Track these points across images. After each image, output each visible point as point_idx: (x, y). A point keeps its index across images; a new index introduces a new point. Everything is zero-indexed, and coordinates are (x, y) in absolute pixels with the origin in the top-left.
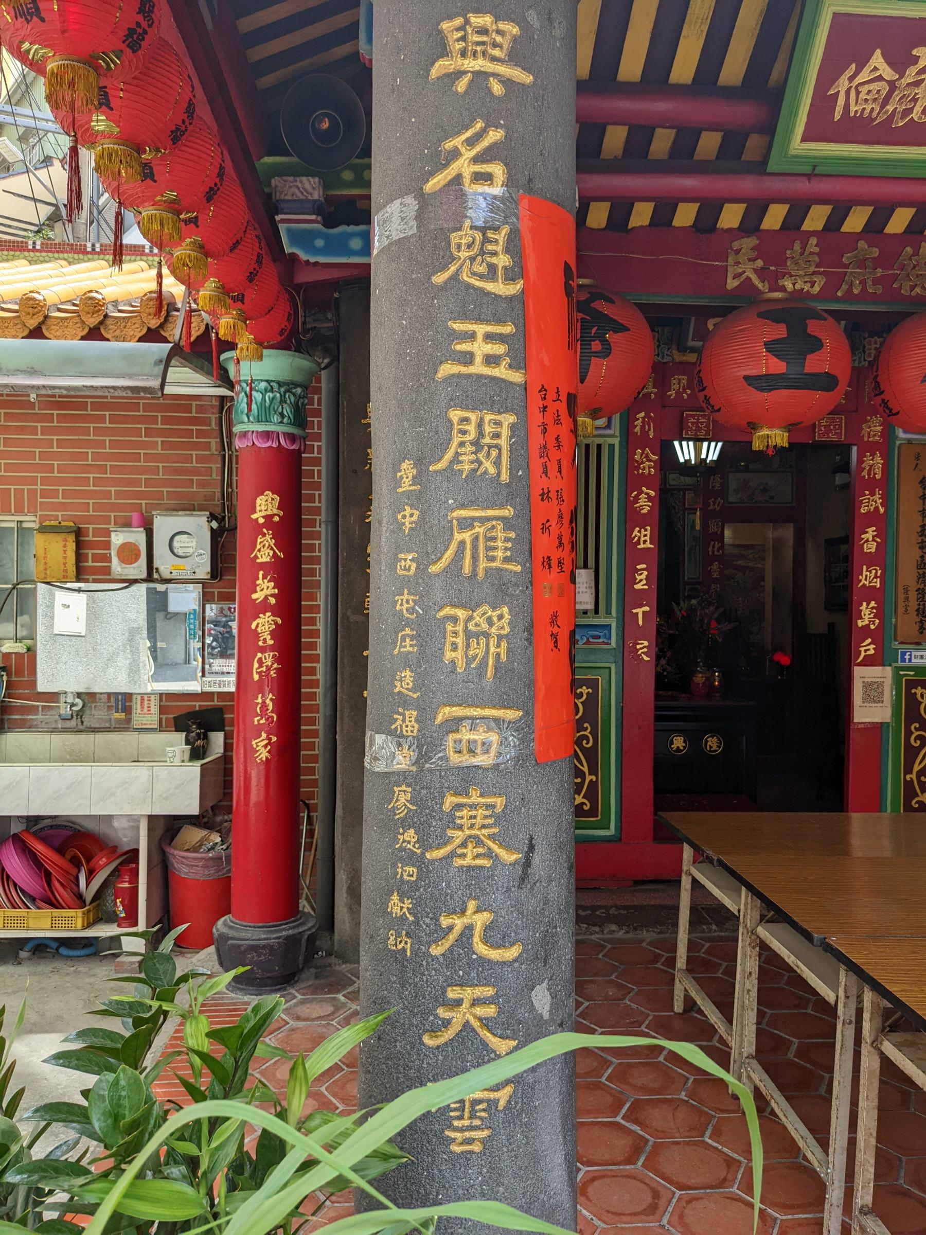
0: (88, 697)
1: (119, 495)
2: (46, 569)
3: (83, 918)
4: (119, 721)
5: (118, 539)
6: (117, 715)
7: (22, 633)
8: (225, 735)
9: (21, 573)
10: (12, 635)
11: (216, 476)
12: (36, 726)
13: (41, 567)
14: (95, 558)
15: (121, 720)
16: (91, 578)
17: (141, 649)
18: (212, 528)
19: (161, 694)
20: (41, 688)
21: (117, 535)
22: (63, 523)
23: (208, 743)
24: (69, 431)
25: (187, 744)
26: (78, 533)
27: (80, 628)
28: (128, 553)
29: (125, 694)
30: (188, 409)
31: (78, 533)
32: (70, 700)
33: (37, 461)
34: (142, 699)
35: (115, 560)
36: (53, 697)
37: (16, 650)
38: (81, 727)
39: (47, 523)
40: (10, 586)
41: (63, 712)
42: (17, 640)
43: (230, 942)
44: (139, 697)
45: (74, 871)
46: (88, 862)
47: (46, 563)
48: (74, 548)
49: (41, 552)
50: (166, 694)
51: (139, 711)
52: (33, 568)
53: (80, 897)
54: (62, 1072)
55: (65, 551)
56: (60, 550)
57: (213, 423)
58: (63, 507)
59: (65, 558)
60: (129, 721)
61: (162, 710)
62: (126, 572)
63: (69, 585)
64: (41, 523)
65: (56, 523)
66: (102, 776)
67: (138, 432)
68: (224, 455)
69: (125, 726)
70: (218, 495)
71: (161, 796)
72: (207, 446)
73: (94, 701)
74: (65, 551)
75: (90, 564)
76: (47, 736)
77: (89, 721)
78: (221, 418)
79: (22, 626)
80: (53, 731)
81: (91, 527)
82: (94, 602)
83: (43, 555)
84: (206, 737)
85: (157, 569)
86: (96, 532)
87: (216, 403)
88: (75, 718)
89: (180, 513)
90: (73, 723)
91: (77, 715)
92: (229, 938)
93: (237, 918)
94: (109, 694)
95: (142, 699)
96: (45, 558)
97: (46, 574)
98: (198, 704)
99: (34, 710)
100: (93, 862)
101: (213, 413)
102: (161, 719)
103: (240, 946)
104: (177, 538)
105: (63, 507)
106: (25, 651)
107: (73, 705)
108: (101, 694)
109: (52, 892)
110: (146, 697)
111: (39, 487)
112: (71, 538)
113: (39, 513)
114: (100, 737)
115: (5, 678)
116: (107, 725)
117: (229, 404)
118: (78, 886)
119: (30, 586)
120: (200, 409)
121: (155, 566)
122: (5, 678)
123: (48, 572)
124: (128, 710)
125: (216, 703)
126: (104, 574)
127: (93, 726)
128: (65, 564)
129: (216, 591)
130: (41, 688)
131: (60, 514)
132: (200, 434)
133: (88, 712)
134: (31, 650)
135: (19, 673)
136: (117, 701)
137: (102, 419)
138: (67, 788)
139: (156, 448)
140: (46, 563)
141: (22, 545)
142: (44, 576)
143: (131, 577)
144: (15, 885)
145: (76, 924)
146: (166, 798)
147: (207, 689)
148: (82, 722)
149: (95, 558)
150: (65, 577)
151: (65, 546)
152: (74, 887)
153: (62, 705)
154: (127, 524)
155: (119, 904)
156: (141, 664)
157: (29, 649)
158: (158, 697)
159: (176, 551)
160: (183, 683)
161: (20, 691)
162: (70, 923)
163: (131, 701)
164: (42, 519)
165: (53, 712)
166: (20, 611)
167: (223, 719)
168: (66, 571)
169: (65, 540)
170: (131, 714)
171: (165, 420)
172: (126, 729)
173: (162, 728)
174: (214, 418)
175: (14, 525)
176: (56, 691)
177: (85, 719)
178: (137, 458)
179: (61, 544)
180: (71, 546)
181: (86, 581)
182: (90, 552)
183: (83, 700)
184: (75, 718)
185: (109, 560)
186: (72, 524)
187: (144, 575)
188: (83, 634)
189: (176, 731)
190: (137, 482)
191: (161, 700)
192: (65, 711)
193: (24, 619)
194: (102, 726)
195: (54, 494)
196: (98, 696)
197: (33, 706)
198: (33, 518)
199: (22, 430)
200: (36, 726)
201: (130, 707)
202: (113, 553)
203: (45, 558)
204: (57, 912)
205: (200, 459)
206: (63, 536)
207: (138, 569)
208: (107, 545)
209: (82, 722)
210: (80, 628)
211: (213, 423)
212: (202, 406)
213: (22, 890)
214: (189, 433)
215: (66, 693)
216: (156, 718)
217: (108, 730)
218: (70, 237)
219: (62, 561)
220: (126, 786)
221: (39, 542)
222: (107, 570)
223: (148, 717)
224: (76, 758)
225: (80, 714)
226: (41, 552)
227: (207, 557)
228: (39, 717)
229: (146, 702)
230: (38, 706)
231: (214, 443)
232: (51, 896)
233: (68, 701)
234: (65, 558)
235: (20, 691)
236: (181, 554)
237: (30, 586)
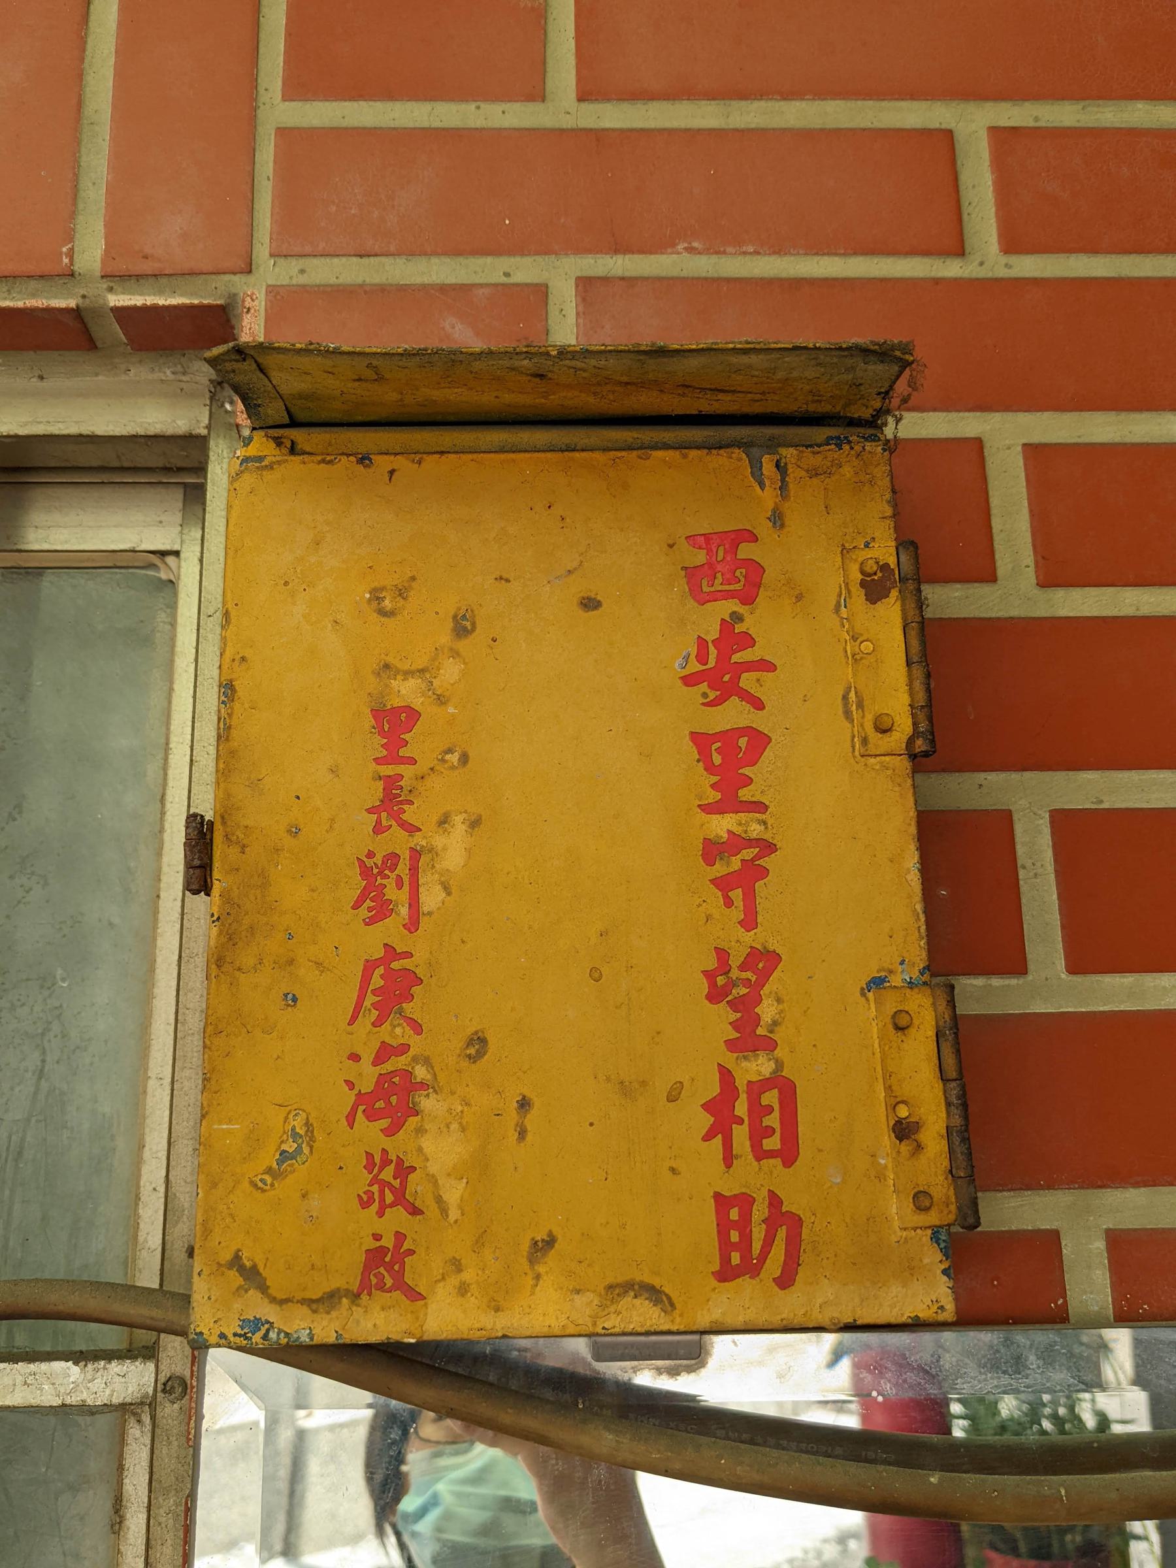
2: (392, 1099)
13: (314, 1056)
47: (392, 986)
49: (321, 781)
54: (772, 1350)
55: (730, 760)
59: (740, 870)
74: (730, 760)
83: (356, 834)
89: (915, 644)
96: (380, 884)
97: (391, 1185)
128: (738, 984)
140: (392, 986)
142: (348, 1228)
151: (724, 668)
160: (377, 279)
169: (726, 568)
179: (665, 630)
203: (380, 884)
206: (696, 489)
219: (686, 924)
234: (740, 870)
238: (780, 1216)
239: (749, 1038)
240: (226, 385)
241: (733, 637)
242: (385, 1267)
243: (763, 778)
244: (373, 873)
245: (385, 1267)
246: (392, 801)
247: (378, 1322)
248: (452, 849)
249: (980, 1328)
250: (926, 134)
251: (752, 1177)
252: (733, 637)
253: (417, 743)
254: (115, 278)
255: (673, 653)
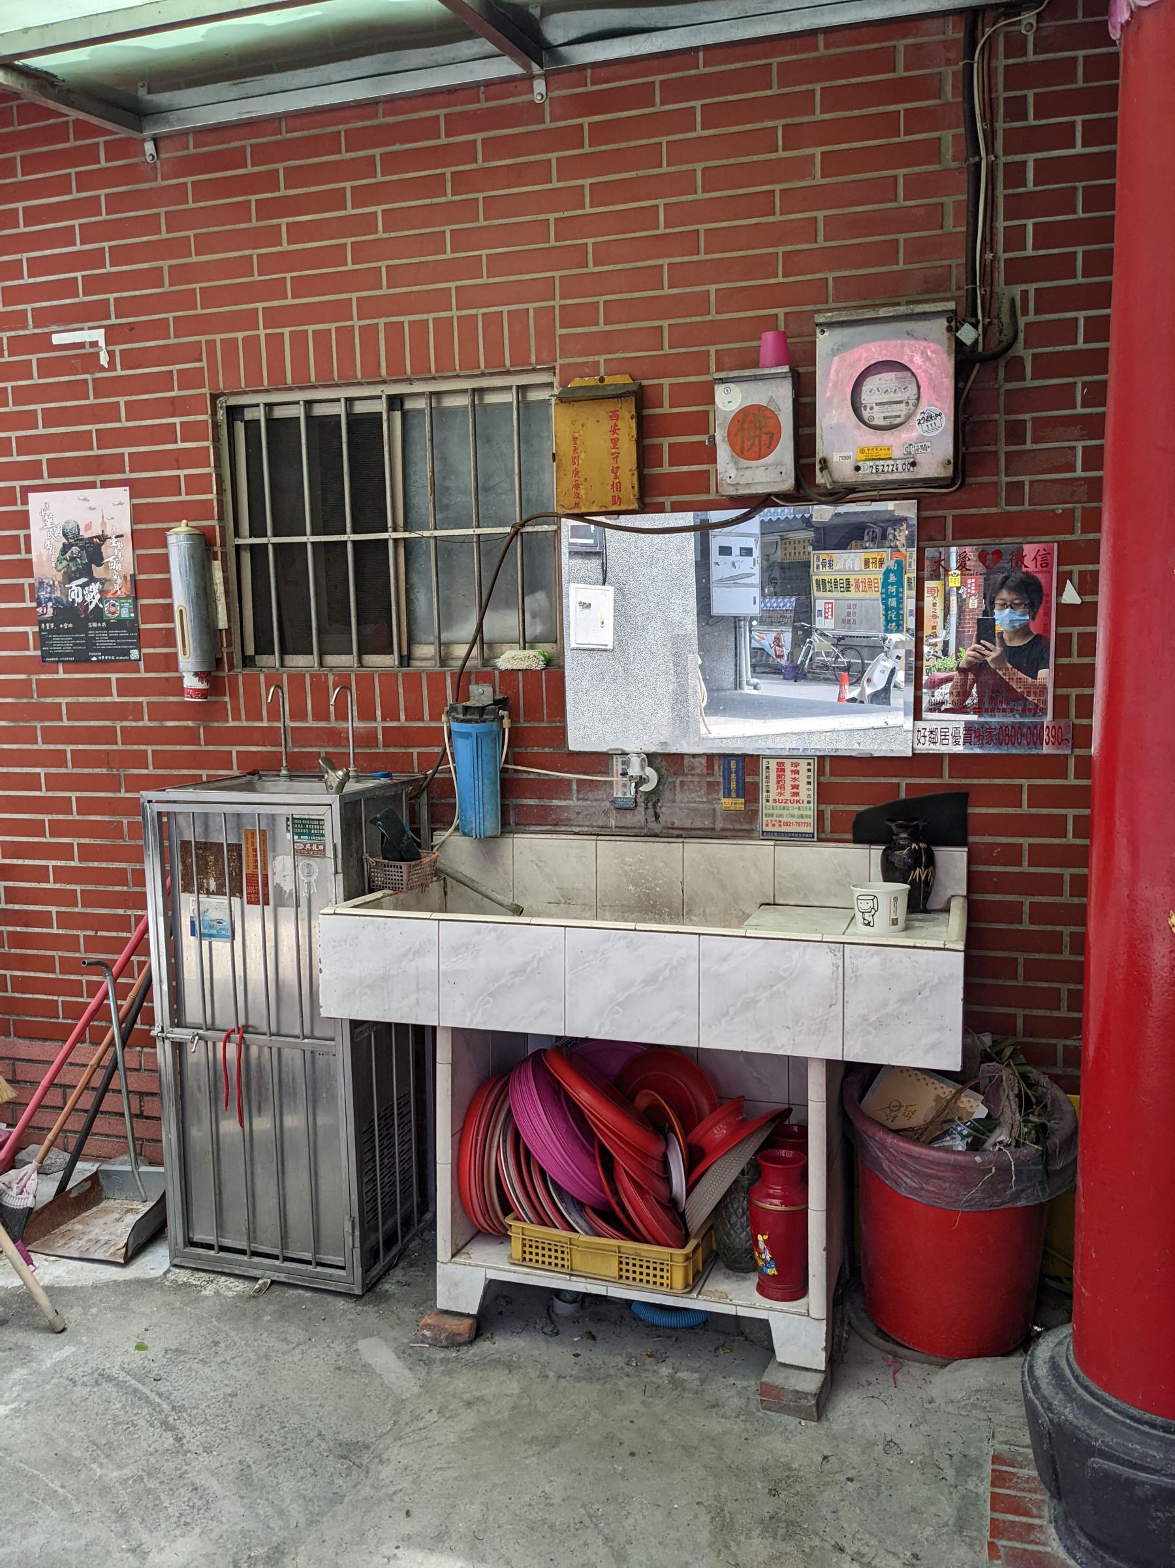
0: (667, 763)
1: (727, 300)
2: (577, 486)
3: (686, 1268)
4: (730, 815)
5: (729, 400)
6: (727, 803)
7: (535, 629)
8: (969, 853)
9: (529, 501)
10: (516, 633)
11: (953, 226)
12: (568, 822)
13: (568, 481)
14: (680, 455)
15: (736, 813)
16: (667, 500)
17: (690, 668)
18: (959, 343)
19: (821, 759)
20: (574, 745)
21: (728, 391)
22: (609, 380)
23: (934, 873)
24: (618, 160)
25: (887, 878)
26: (641, 398)
27: (606, 638)
28: (753, 432)
29: (744, 756)
30: (885, 61)
31: (641, 398)
32: (635, 770)
33: (553, 243)
34: (781, 770)
35: (723, 452)
36: (598, 761)
37: (524, 665)
38: (653, 825)
39: (577, 382)
40: (508, 530)
41: (618, 793)
42: (526, 643)
43: (1097, 1462)
44: (773, 764)
45: (656, 1150)
46: (687, 1129)
47: (576, 473)
48: (634, 433)
49: (566, 448)
50: (834, 758)
51: (773, 795)
52: (553, 488)
53: (673, 1208)
55: (615, 442)
56: (599, 444)
57: (948, 88)
58: (606, 342)
59: (616, 456)
60: (752, 815)
61: (824, 793)
62: (748, 476)
63: (624, 520)
64: (563, 385)
65: (593, 381)
66: (724, 960)
67: (766, 140)
68: (978, 166)
69: (744, 826)
70: (958, 274)
71: (865, 1018)
72: (932, 151)
73: (680, 772)
74: (615, 442)
75: (666, 469)
76: (589, 844)
77: (671, 813)
78: (970, 67)
79: (534, 616)
80: (601, 832)
81: (666, 382)
82: (624, 597)
84: (931, 862)
85: (824, 462)
86: (680, 394)
87: (954, 32)
88: (641, 809)
90: (638, 818)
91: (647, 801)
92: (1092, 1451)
93: (1079, 1363)
94: (710, 757)
95: (781, 770)
96: (575, 460)
97: (577, 496)
98: (903, 782)
99: (561, 789)
100: (697, 1133)
101: (948, 62)
102: (820, 815)
103: (1131, 1483)
104: (871, 383)
105: (606, 342)
106: (541, 665)
107: (641, 781)
108: (694, 756)
109: (616, 1193)
110: (788, 762)
111: (557, 302)
112: (627, 411)
113: (560, 361)
114: (694, 850)
115: (506, 723)
116: (707, 823)
117: (989, 31)
118: (668, 1180)
119: (546, 528)
120: (917, 56)
121: (820, 453)
122: (506, 723)
123: (582, 492)
124: (750, 793)
125: (946, 780)
126: (694, 491)
127: (677, 824)
128: (615, 471)
129: (949, 514)
130: (574, 745)
131: (601, 359)
132: (916, 120)
133: (668, 795)
134: (554, 668)
135: (533, 712)
136: (727, 771)
137: (684, 120)
138: (646, 983)
139: (807, 174)
140: (576, 473)
141: (527, 441)
143: (760, 490)
144: (543, 1174)
145: (670, 1278)
146: (880, 1024)
147: (926, 747)
148: (657, 816)
149: (680, 455)
150: (616, 500)
151: (614, 430)
152: (661, 1186)
153: (617, 779)
154: (745, 364)
155: (762, 1245)
156: (690, 691)
157: (548, 662)
158: (814, 766)
159: (866, 414)
161: (536, 750)
162: (653, 1277)
163: (756, 772)
164: (568, 372)
165: (600, 794)
166: (531, 584)
167: (965, 817)
168: (617, 486)
169: (615, 416)
170: (756, 800)
171: (832, 100)
172: (747, 834)
173: (824, 833)
174: (950, 74)
175: (509, 398)
176: (604, 750)
177: (665, 810)
178: (765, 203)
179: (607, 425)
180: (628, 428)
181: (660, 509)
182: (666, 442)
183: (657, 770)
184: (641, 809)
185: (710, 455)
186: (626, 379)
187: (787, 483)
188: (610, 647)
189: (855, 842)
190: (764, 266)
191: (821, 771)
192: (623, 791)
193: (537, 600)
194: (698, 824)
195: (587, 315)
196: (686, 760)
197: (561, 780)
198: (544, 378)
199: (518, 174)
200: (568, 822)
201: (756, 785)
202: (720, 436)
204: (629, 1245)
205: (916, 187)
206: (610, 406)
207: (774, 470)
208: (702, 422)
209: (657, 816)
210: (606, 638)
211: (948, 88)
212: (919, 47)
213: (554, 1183)
214: (888, 125)
215: (624, 754)
216: (810, 811)
217: (710, 834)
218: (544, 378)
219: (609, 463)
220: (780, 987)
221: (560, 424)
222: (702, 482)
223: (794, 809)
224: (655, 905)
225: (653, 798)
226: (566, 448)
227: (945, 424)
228: (573, 802)
229: (788, 775)
230: (570, 781)
231: (949, 138)
232: (613, 1201)
233: (631, 772)
234: (616, 456)
235: (536, 750)
236: (879, 421)
237: (546, 528)
238: (619, 498)
239: (616, 478)
240: (445, 636)
241: (615, 425)
242: (577, 505)
243: (619, 444)
244: (573, 459)
245: (577, 505)
246: (575, 449)
247: (576, 511)
248: (583, 455)
249: (430, 1188)
250: (703, 175)
251: (616, 493)
252: (615, 425)
253: (578, 442)
254: (538, 364)
255: (608, 428)
